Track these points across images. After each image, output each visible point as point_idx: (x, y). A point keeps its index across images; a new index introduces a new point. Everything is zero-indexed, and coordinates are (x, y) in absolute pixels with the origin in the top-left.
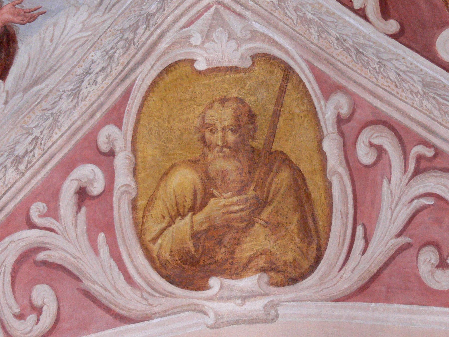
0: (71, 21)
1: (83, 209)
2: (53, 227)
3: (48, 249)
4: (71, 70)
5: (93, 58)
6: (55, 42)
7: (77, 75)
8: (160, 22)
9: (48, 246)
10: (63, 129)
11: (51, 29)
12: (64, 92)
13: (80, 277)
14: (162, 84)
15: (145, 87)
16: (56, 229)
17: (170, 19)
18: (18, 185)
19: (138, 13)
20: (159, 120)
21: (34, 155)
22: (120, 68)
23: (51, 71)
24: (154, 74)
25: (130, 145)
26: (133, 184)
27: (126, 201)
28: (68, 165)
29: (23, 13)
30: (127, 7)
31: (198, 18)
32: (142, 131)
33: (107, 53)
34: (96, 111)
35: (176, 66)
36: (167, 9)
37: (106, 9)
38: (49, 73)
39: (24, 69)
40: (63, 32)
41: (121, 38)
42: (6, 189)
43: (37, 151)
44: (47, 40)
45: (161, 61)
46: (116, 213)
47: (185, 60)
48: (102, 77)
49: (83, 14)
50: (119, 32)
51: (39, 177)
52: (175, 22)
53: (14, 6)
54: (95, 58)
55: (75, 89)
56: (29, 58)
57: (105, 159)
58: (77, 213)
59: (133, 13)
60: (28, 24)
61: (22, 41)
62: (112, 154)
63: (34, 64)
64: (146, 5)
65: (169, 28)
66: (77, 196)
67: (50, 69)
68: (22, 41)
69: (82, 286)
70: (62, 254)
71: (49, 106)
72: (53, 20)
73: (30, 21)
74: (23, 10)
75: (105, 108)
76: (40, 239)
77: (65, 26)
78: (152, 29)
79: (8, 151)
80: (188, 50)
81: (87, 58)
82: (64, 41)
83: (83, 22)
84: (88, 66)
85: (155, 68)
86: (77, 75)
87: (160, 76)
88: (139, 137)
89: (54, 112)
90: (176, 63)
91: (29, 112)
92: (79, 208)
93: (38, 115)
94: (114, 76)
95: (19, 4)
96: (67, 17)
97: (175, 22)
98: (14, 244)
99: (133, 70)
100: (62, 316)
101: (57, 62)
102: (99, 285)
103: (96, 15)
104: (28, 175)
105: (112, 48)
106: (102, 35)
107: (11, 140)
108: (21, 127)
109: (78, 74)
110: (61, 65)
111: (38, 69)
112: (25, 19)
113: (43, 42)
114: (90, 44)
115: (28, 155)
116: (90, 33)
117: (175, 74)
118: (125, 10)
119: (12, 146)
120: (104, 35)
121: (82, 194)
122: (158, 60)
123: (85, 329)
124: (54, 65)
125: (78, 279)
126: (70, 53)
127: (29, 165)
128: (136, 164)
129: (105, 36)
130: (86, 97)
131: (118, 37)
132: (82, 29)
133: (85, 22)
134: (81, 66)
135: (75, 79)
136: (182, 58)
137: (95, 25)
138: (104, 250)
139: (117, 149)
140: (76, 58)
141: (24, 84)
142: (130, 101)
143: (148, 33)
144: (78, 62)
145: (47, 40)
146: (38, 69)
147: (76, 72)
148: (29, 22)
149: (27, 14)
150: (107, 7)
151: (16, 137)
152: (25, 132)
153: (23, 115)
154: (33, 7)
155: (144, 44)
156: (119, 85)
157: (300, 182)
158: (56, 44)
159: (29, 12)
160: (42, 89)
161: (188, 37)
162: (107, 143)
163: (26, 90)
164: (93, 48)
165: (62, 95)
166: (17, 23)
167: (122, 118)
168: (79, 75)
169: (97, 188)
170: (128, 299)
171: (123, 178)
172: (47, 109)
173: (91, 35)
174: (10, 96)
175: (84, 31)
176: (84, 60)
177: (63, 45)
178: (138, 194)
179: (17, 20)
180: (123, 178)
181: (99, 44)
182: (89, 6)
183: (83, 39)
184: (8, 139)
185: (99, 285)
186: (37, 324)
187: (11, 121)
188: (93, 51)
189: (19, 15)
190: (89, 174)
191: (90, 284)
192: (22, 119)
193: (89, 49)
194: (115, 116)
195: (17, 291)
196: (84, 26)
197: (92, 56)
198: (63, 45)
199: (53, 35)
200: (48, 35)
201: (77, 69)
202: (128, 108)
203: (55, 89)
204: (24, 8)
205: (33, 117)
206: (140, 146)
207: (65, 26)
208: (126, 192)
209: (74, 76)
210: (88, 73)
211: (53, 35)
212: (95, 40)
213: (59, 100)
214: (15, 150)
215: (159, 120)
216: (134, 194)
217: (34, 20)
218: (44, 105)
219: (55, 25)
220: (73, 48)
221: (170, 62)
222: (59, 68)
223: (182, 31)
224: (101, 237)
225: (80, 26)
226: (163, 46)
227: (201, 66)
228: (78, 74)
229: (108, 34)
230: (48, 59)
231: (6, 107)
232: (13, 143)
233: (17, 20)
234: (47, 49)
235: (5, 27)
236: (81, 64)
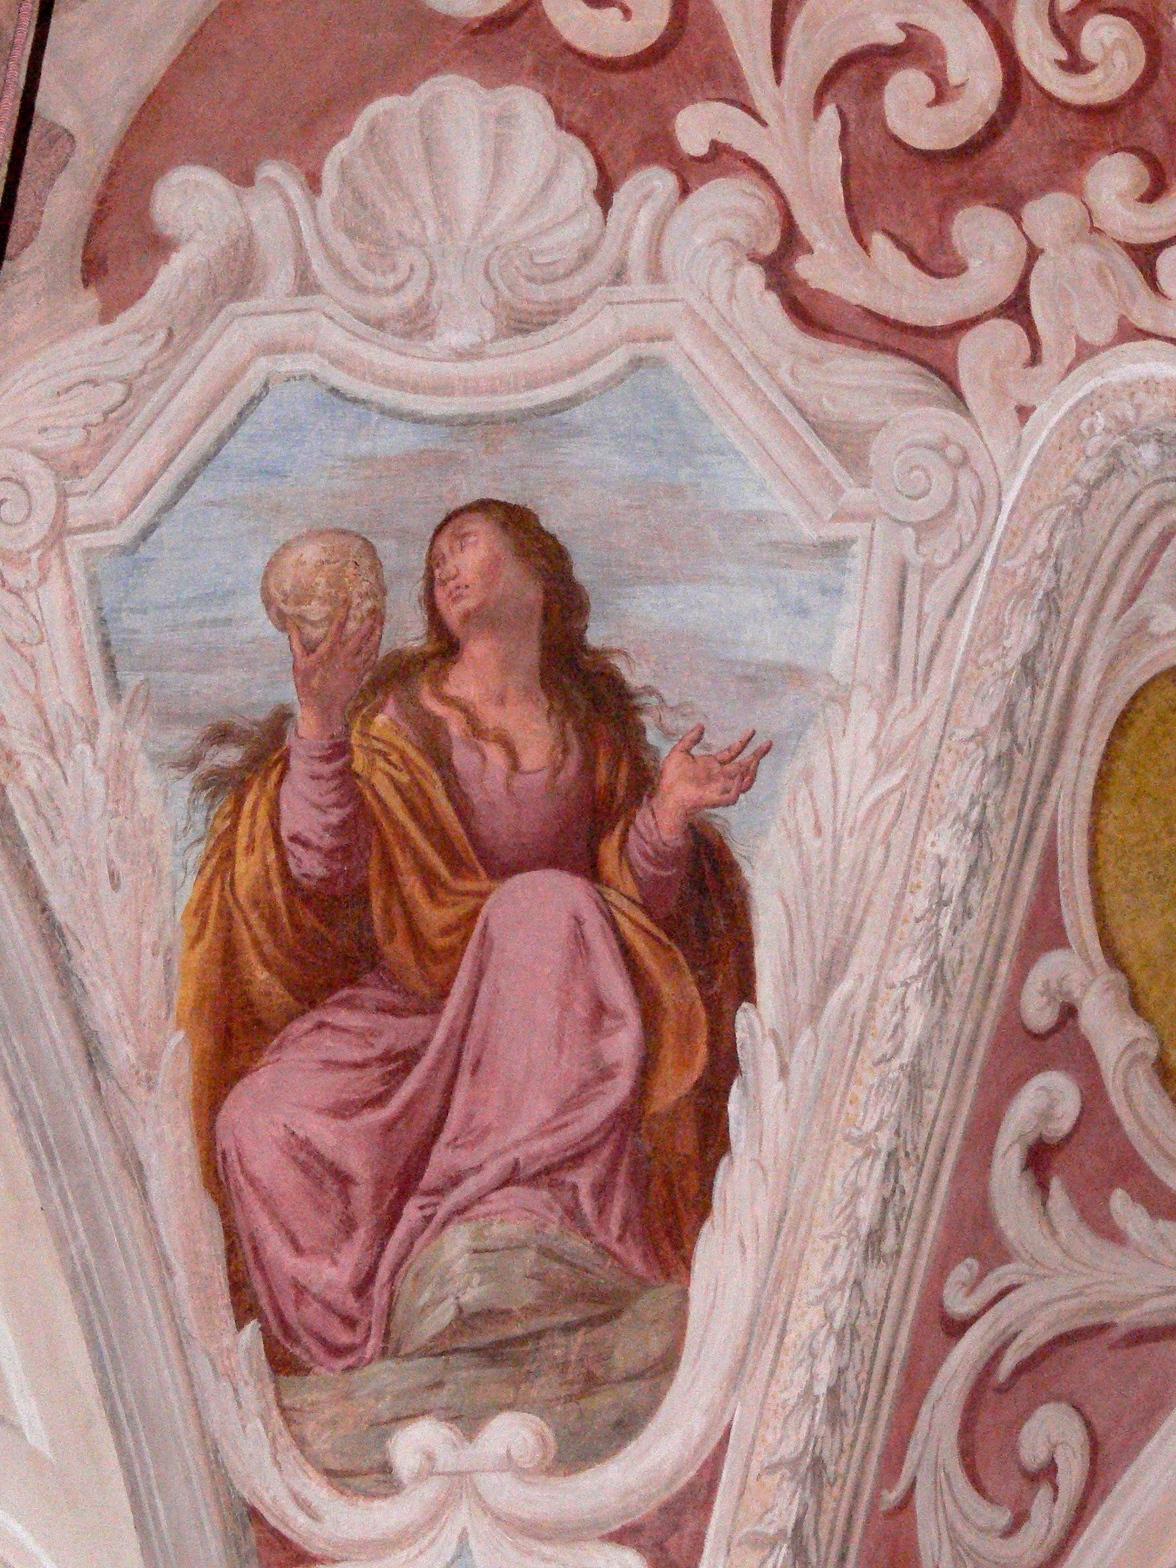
0: (844, 750)
1: (1055, 1184)
2: (1005, 1283)
3: (1015, 1335)
4: (898, 908)
5: (935, 850)
6: (827, 826)
7: (917, 921)
8: (1057, 648)
9: (1013, 1329)
10: (939, 1079)
11: (803, 793)
12: (906, 985)
13: (1106, 1318)
14: (1122, 768)
15: (1082, 821)
16: (1014, 1279)
17: (1080, 620)
18: (897, 1288)
19: (997, 666)
20: (1147, 848)
21: (903, 1193)
22: (1010, 825)
23: (852, 928)
24: (1092, 763)
25: (1101, 959)
26: (1142, 1031)
27: (1142, 1079)
29: (716, 767)
30: (965, 662)
31: (1149, 572)
32: (1117, 900)
33: (966, 825)
34: (996, 963)
35: (1140, 704)
36: (1063, 605)
37: (915, 679)
38: (849, 939)
39: (786, 945)
40: (836, 793)
41: (984, 761)
42: (875, 1322)
43: (906, 1179)
44: (808, 833)
45: (1099, 721)
46: (1130, 1126)
47: (1153, 680)
48: (978, 885)
49: (863, 722)
50: (972, 746)
51: (933, 1223)
52: (1094, 618)
53: (688, 751)
54: (941, 849)
55: (928, 967)
56: (786, 906)
57: (1063, 1041)
58: (1044, 1204)
59: (987, 671)
60: (742, 797)
61: (748, 859)
63: (804, 922)
64: (1009, 633)
65: (1086, 641)
66: (1029, 1174)
67: (847, 924)
68: (748, 859)
69: (1115, 1335)
70: (1047, 1315)
71: (887, 1048)
72: (799, 764)
73: (744, 785)
74: (714, 757)
75: (1010, 945)
76: (992, 1334)
77: (833, 771)
78: (1048, 676)
79: (844, 1232)
80: (1156, 650)
81: (923, 855)
82: (848, 824)
83: (873, 745)
84: (933, 880)
85: (1089, 749)
86: (917, 921)
87: (1109, 756)
88: (1114, 921)
89: (905, 1061)
90: (1134, 699)
91: (847, 1085)
92: (1043, 1187)
93: (872, 1086)
94: (1003, 858)
95: (697, 741)
96: (830, 743)
97: (1094, 618)
98: (942, 1405)
99: (1041, 799)
100: (1099, 1431)
101: (856, 895)
102: (1152, 1296)
103: (895, 710)
104: (908, 1246)
105: (972, 804)
106: (933, 770)
107: (838, 1189)
108: (847, 1138)
109: (918, 913)
110: (869, 902)
111: (819, 933)
112: (730, 782)
113: (800, 842)
114: (915, 805)
115: (891, 1206)
116: (903, 772)
117: (1143, 722)
118: (962, 670)
119: (848, 1212)
120: (938, 766)
121: (1040, 1158)
122: (1089, 725)
123: (1161, 1407)
124: (853, 907)
125: (1102, 1328)
126: (878, 854)
127: (902, 1224)
128: (1132, 984)
129: (941, 770)
130: (961, 963)
131: (974, 762)
132: (878, 767)
133: (880, 743)
134: (919, 887)
135: (918, 934)
136: (1146, 677)
137: (904, 744)
139: (1077, 994)
140: (897, 863)
141: (803, 992)
142: (1062, 868)
143: (1042, 694)
144: (906, 876)
145: (808, 833)
146: (819, 933)
147: (911, 909)
148: (744, 792)
149: (728, 767)
150: (915, 671)
151: (846, 1177)
152: (859, 1153)
153: (837, 1098)
154: (733, 739)
155: (1043, 724)
156: (1021, 865)
158: (834, 837)
159: (733, 758)
160: (852, 996)
161: (1141, 627)
162: (1049, 1003)
163: (815, 1011)
164: (926, 817)
165: (904, 996)
166: (715, 806)
167: (1060, 919)
168: (923, 917)
171: (1111, 1032)
172: (886, 1059)
173: (907, 776)
174: (784, 1038)
175: (887, 771)
176: (918, 863)
177: (851, 835)
178: (1162, 1044)
179: (712, 793)
181: (937, 798)
182: (870, 688)
183: (891, 799)
184: (831, 1191)
185: (1152, 1296)
186: (1055, 1499)
187: (816, 1129)
188: (930, 828)
189: (710, 778)
190: (1047, 1100)
191: (1134, 1312)
192: (839, 1112)
193: (918, 828)
194: (1044, 931)
195: (988, 1484)
196: (879, 756)
197: (933, 844)
198: (851, 835)
199: (816, 812)
200: (803, 811)
201: (909, 898)
202: (1062, 887)
203: (882, 982)
204: (714, 751)
205: (863, 1097)
206: (1124, 940)
207: (833, 771)
208: (1134, 1061)
209: (912, 922)
210: (943, 903)
211: (816, 812)
212: (923, 793)
213: (904, 1017)
214: (857, 1220)
215: (1147, 848)
216: (1152, 1051)
217: (752, 780)
218: (878, 1046)
219: (808, 776)
220: (878, 838)
221: (1120, 707)
222: (866, 911)
223: (1121, 622)
224: (1119, 1201)
225: (871, 759)
228: (918, 915)
229: (948, 758)
230: (832, 893)
231: (786, 1085)
232: (846, 1199)
233: (712, 793)
234: (815, 862)
235: (691, 826)
236: (914, 878)
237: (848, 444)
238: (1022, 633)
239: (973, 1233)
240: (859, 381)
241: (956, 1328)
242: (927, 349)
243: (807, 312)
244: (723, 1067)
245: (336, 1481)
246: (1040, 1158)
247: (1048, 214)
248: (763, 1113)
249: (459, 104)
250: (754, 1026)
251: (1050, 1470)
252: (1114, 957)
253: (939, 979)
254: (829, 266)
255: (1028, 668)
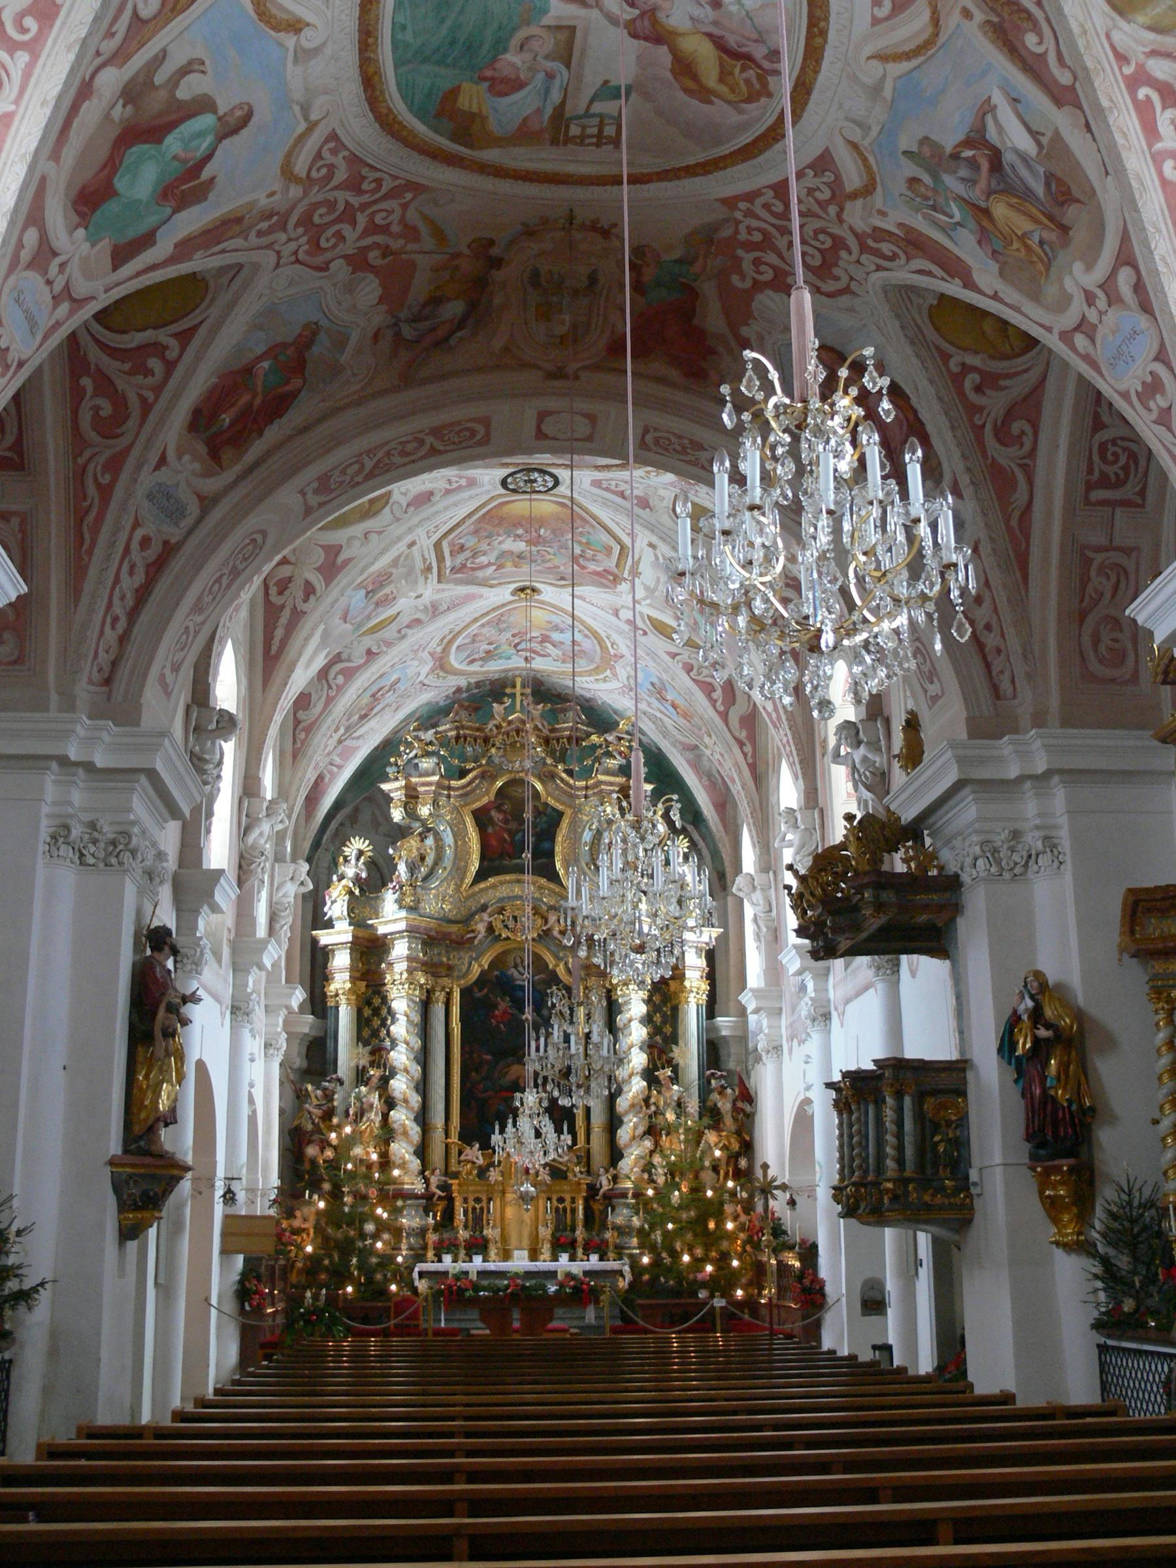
28: (962, 394)
57: (966, 369)
62: (963, 365)
121: (978, 389)
138: (1007, 382)
157: (690, 84)
169: (976, 377)
170: (1033, 376)
171: (975, 361)
180: (975, 361)
190: (971, 380)
224: (1002, 383)
226: (919, 321)
227: (935, 302)
237: (851, 310)
238: (897, 324)
239: (973, 410)
240: (844, 300)
241: (983, 426)
242: (847, 290)
243: (829, 295)
244: (915, 412)
245: (385, 871)
246: (978, 389)
247: (841, 263)
248: (924, 415)
249: (759, 297)
250: (914, 401)
251: (1023, 433)
252: (965, 349)
253: (932, 382)
254: (825, 288)
255: (902, 327)
